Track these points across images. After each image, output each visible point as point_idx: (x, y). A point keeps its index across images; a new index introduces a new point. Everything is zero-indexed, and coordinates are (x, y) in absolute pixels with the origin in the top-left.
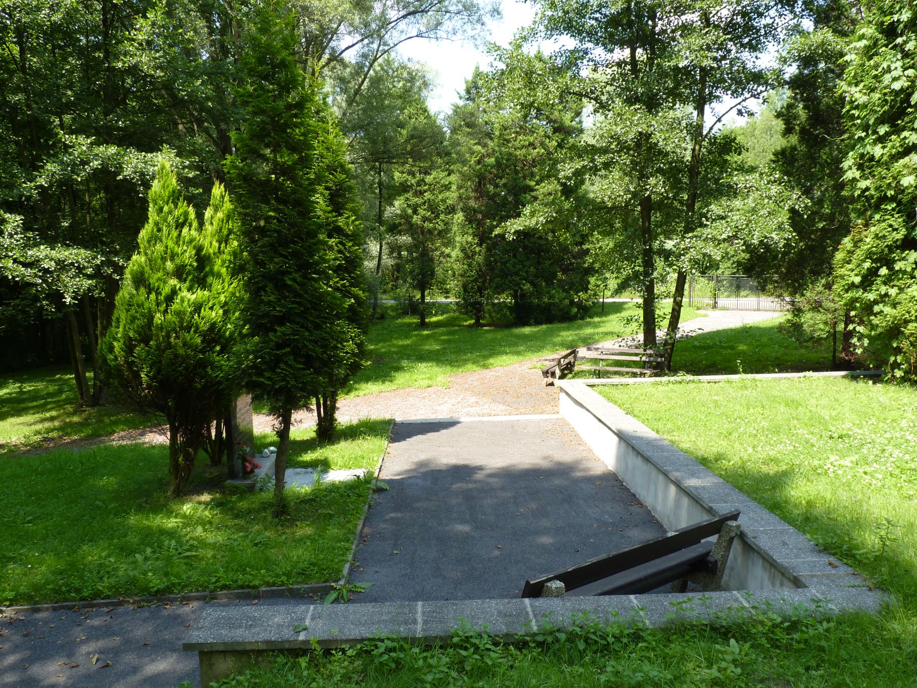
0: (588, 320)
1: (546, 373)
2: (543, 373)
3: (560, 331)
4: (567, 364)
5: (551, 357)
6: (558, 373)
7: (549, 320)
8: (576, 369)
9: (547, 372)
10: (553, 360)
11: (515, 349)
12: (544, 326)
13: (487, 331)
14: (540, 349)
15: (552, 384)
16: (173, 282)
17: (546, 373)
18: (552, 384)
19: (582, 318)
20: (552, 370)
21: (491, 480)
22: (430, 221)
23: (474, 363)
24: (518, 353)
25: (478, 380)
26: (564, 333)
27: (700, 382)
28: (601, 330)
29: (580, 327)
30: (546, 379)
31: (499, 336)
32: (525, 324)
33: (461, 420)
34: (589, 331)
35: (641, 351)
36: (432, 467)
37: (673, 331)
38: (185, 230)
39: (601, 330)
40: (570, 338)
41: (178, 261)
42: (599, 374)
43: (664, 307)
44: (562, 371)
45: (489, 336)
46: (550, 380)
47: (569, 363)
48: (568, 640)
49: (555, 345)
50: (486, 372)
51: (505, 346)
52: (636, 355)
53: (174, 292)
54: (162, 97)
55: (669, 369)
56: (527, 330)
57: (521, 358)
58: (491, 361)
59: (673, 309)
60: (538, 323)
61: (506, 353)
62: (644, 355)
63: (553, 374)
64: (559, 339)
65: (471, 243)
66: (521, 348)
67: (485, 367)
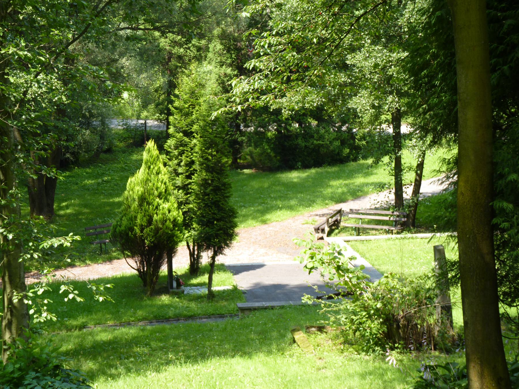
0: (362, 162)
1: (317, 230)
2: (315, 229)
3: (329, 180)
4: (335, 222)
5: (321, 212)
6: (327, 229)
7: (318, 164)
8: (342, 224)
9: (318, 229)
10: (323, 215)
11: (286, 203)
12: (313, 171)
13: (249, 175)
14: (310, 203)
15: (322, 238)
16: (158, 200)
17: (317, 230)
18: (322, 238)
19: (355, 160)
20: (322, 227)
21: (294, 289)
22: (181, 45)
23: (253, 219)
24: (291, 208)
25: (260, 234)
26: (335, 183)
27: (417, 238)
28: (372, 179)
29: (351, 175)
30: (317, 235)
31: (266, 185)
32: (292, 168)
33: (265, 263)
34: (359, 180)
35: (389, 212)
36: (262, 285)
37: (416, 196)
38: (160, 175)
39: (372, 179)
40: (340, 190)
41: (159, 190)
42: (358, 231)
43: (409, 177)
44: (330, 227)
45: (255, 184)
46: (320, 235)
47: (336, 220)
48: (318, 43)
49: (324, 198)
50: (265, 227)
51: (276, 199)
52: (387, 215)
53: (159, 205)
54: (102, 74)
55: (414, 226)
56: (294, 176)
57: (294, 213)
58: (268, 216)
59: (416, 180)
60: (306, 166)
61: (281, 209)
62: (391, 216)
63: (323, 231)
64: (329, 190)
65: (230, 75)
66: (293, 202)
67: (264, 222)
